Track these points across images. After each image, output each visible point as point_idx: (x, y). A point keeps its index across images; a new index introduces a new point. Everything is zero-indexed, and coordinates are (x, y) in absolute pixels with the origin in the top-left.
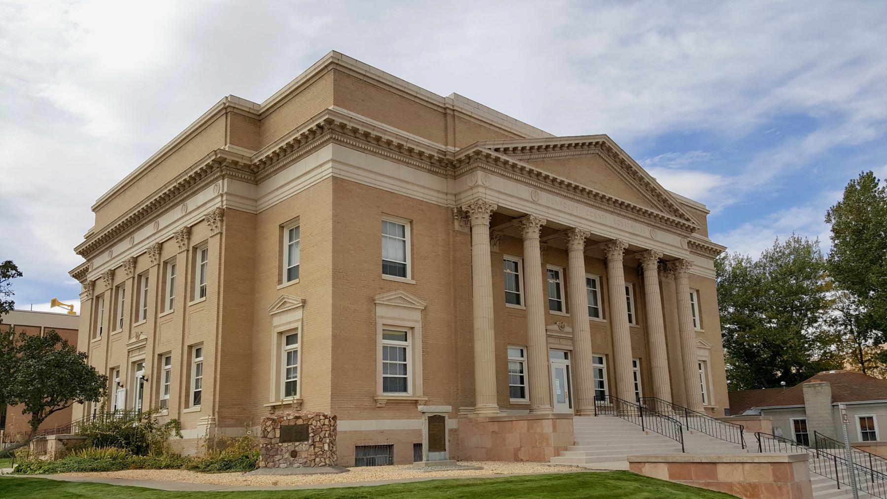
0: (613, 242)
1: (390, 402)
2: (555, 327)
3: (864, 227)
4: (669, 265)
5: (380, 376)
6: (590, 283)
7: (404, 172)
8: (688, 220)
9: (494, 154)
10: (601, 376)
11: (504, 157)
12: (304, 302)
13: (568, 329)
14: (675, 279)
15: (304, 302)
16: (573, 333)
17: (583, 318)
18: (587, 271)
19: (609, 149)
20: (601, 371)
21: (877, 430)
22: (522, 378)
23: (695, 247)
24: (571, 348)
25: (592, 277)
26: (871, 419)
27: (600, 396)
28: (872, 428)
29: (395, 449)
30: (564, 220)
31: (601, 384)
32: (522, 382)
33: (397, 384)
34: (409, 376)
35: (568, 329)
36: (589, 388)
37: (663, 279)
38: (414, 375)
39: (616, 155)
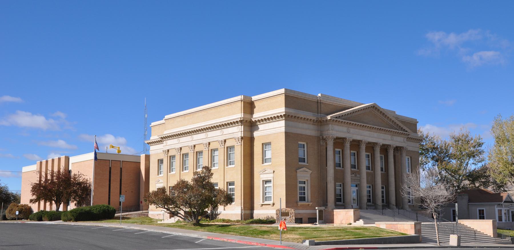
0: (376, 144)
1: (302, 205)
2: (353, 175)
3: (465, 141)
4: (399, 149)
5: (299, 196)
6: (368, 156)
7: (305, 126)
8: (406, 131)
9: (335, 119)
10: (370, 193)
11: (339, 120)
12: (274, 172)
13: (358, 176)
14: (401, 154)
15: (274, 172)
16: (360, 177)
17: (364, 171)
18: (366, 152)
19: (376, 108)
20: (370, 191)
21: (485, 215)
22: (340, 195)
23: (409, 139)
24: (359, 183)
25: (368, 154)
26: (483, 210)
27: (369, 201)
28: (483, 214)
29: (303, 219)
30: (358, 138)
31: (370, 196)
32: (340, 196)
33: (303, 199)
34: (306, 196)
35: (358, 176)
36: (365, 199)
37: (396, 154)
38: (308, 194)
39: (378, 110)
